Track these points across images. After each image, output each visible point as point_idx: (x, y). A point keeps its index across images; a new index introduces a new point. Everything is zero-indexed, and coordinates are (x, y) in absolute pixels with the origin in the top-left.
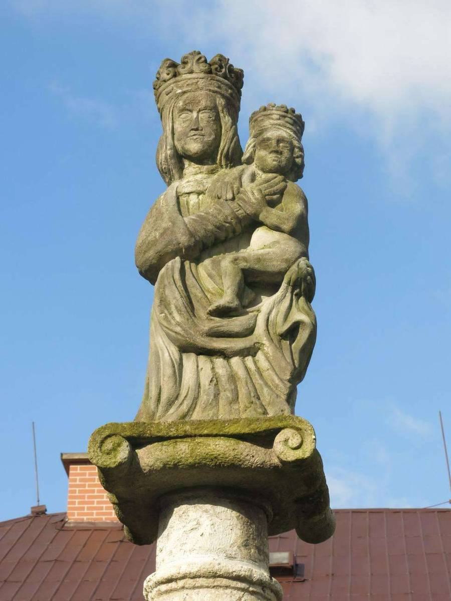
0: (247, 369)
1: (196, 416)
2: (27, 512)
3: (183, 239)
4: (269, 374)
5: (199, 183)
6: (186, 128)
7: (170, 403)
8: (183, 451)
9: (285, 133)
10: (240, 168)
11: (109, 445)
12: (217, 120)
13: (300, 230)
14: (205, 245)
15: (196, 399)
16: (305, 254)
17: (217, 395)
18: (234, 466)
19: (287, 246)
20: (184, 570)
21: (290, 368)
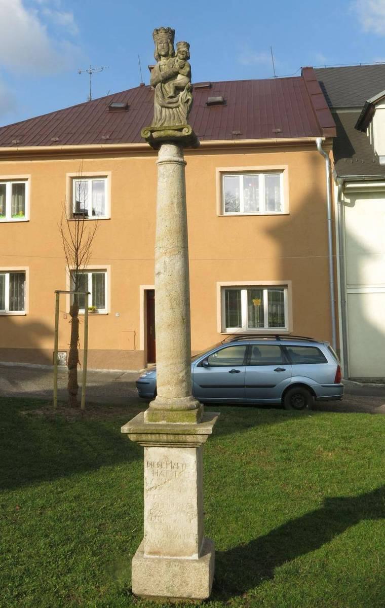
0: (177, 111)
1: (165, 125)
2: (139, 85)
3: (161, 79)
4: (182, 112)
5: (164, 62)
6: (161, 48)
7: (160, 120)
8: (162, 133)
9: (185, 49)
10: (174, 58)
11: (146, 132)
12: (168, 46)
13: (189, 75)
14: (167, 79)
15: (165, 119)
16: (190, 81)
17: (170, 118)
18: (174, 137)
19: (186, 79)
20: (164, 160)
21: (187, 111)
